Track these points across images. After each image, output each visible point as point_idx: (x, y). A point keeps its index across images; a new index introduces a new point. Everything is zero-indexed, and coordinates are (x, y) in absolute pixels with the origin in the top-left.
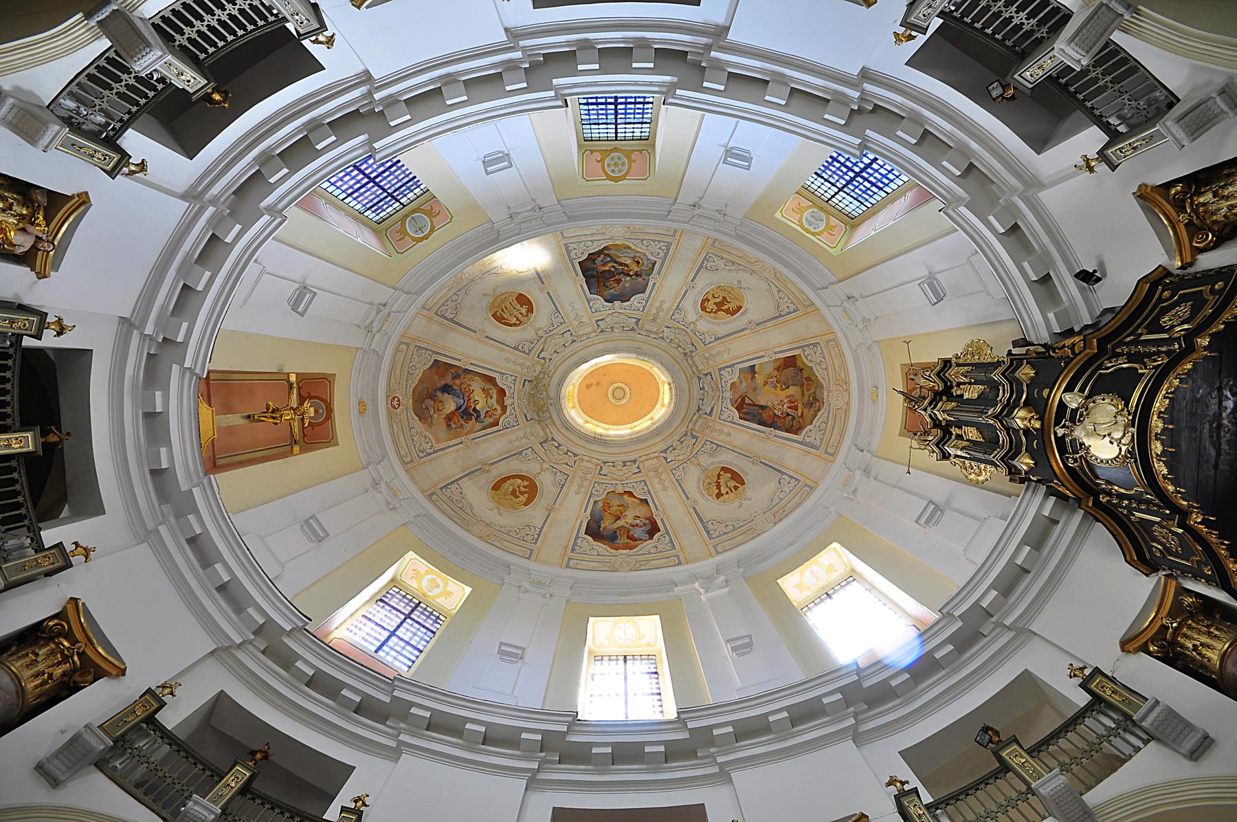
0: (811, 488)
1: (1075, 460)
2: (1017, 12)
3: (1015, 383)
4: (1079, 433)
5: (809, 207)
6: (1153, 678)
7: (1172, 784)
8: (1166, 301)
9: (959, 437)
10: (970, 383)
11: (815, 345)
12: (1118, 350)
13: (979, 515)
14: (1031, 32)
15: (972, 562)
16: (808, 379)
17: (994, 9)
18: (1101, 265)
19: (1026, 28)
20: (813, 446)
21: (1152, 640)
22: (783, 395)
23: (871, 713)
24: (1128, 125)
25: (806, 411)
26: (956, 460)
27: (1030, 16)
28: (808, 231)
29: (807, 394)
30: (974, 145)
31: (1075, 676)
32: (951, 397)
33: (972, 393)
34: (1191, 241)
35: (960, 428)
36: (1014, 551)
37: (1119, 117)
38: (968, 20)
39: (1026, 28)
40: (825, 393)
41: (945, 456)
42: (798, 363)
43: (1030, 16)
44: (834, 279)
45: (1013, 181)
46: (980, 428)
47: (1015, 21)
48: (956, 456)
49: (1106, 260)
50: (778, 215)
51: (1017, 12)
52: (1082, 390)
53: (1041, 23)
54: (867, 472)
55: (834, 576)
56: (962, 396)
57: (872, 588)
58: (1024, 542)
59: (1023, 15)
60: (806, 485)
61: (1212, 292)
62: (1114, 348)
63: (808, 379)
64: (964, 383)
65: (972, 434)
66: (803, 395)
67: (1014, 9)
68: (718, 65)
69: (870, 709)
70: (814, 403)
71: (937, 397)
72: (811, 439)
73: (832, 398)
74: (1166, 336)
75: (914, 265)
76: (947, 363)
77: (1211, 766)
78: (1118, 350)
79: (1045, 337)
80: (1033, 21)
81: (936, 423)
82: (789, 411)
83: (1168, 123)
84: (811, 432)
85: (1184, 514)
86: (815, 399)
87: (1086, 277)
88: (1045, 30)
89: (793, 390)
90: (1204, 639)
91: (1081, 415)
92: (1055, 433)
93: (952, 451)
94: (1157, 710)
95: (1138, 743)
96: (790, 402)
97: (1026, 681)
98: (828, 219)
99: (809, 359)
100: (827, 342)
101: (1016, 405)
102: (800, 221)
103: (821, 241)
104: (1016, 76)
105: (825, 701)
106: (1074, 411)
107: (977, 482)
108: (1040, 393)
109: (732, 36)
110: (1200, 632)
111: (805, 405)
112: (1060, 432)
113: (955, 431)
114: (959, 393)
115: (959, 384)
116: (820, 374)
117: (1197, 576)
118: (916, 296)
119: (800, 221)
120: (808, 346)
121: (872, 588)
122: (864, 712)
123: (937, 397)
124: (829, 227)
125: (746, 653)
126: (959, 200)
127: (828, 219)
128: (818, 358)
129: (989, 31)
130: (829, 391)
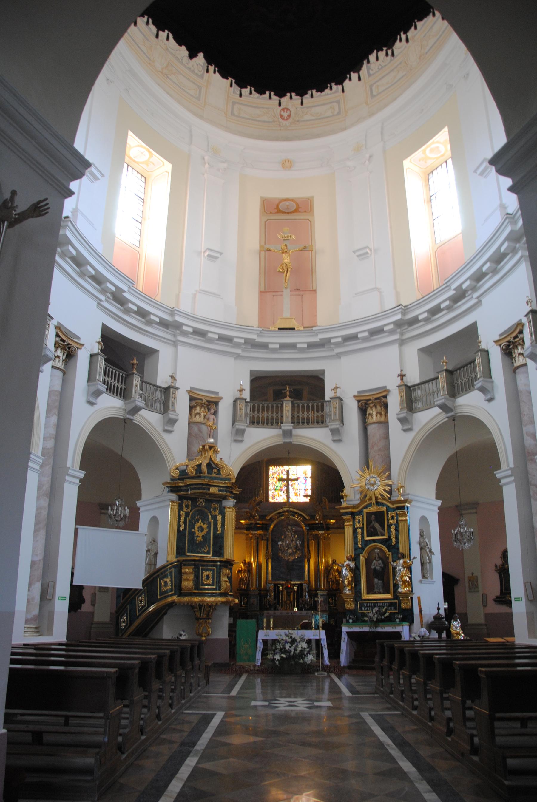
6: (181, 404)
39: (459, 380)
122: (110, 299)
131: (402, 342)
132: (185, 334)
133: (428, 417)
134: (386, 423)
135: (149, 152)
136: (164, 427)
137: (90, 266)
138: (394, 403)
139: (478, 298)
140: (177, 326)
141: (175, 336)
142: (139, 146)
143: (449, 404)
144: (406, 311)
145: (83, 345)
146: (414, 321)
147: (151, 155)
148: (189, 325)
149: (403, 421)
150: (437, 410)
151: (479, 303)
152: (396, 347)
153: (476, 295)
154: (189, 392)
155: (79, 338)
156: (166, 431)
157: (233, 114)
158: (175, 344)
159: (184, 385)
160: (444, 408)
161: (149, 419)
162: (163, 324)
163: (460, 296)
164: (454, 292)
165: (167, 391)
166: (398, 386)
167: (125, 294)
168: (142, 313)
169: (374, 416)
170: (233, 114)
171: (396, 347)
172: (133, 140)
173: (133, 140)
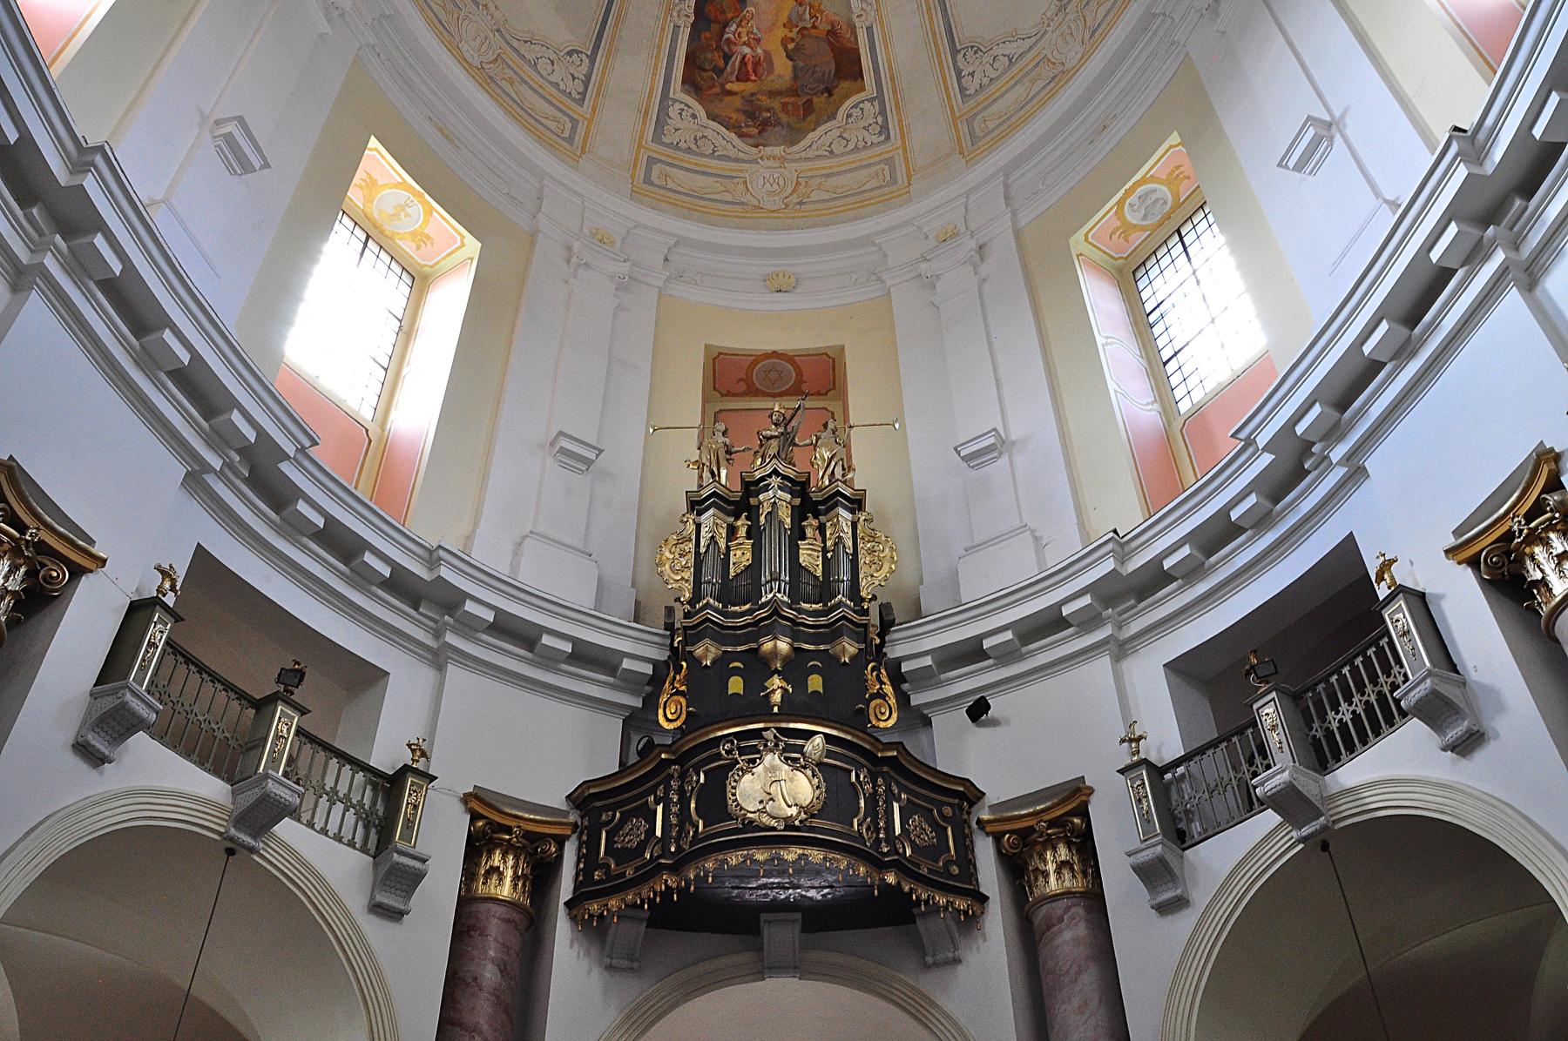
0: (570, 140)
1: (728, 752)
2: (1354, 712)
3: (833, 633)
4: (771, 759)
5: (1176, 195)
6: (440, 835)
7: (334, 895)
8: (940, 813)
9: (732, 532)
10: (825, 550)
11: (885, 128)
12: (880, 781)
13: (584, 523)
14: (1323, 716)
15: (517, 553)
16: (808, 108)
17: (1369, 688)
18: (994, 723)
19: (1331, 714)
20: (660, 124)
21: (490, 823)
22: (773, 44)
23: (238, 482)
24: (1170, 783)
25: (737, 102)
26: (691, 527)
27: (1343, 726)
28: (1128, 193)
29: (776, 104)
30: (1202, 588)
31: (413, 751)
32: (799, 514)
33: (809, 557)
34: (1012, 832)
35: (749, 537)
36: (559, 632)
37: (1183, 775)
38: (1370, 652)
39: (1331, 714)
40: (778, 151)
41: (696, 505)
42: (845, 85)
43: (1343, 726)
44: (1023, 222)
45: (1136, 626)
46: (754, 568)
47: (1344, 706)
48: (698, 526)
49: (998, 729)
50: (1175, 138)
51: (1354, 712)
52: (829, 754)
53: (1329, 734)
54: (624, 285)
55: (407, 246)
56: (803, 537)
57: (407, 331)
58: (575, 641)
59: (1348, 717)
60: (575, 123)
61: (948, 863)
62: (883, 775)
63: (808, 108)
64: (824, 541)
65: (741, 557)
66: (773, 94)
67: (1360, 710)
68: (1475, 255)
69: (246, 481)
70: (755, 123)
71: (799, 487)
72: (674, 120)
73: (768, 170)
74: (898, 831)
75: (1030, 418)
76: (856, 504)
77: (375, 930)
78: (880, 781)
79: (894, 651)
80: (1335, 726)
81: (752, 487)
82: (736, 61)
83: (1159, 848)
84: (689, 117)
85: (674, 869)
86: (764, 125)
87: (978, 710)
88: (1319, 734)
89: (783, 68)
90: (509, 873)
91: (795, 760)
92: (766, 729)
93: (708, 518)
94: (417, 864)
95: (358, 839)
96: (757, 64)
97: (368, 677)
98: (1143, 229)
99: (855, 111)
100: (889, 162)
101: (795, 636)
102: (1153, 179)
103: (1104, 216)
104: (1274, 694)
105: (236, 416)
106: (800, 749)
107: (661, 564)
108: (815, 670)
109: (1513, 298)
110: (515, 867)
111: (750, 99)
112: (769, 735)
113: (742, 524)
114: (809, 532)
115: (821, 529)
116: (821, 136)
117: (588, 859)
118: (976, 423)
119: (1153, 179)
120: (883, 112)
121: (407, 331)
122: (237, 474)
123: (799, 487)
124: (1128, 228)
125: (229, 167)
126: (1122, 559)
127: (1143, 229)
128: (856, 135)
129: (1346, 670)
130: (782, 160)
131: (1121, 649)
132: (470, 627)
133: (1240, 852)
134: (1094, 899)
135: (424, 202)
136: (372, 897)
137: (105, 236)
138: (1118, 830)
139: (1348, 458)
140: (449, 602)
141: (438, 635)
142: (397, 185)
143: (1308, 784)
144: (1127, 549)
145: (104, 561)
146: (1155, 579)
147: (429, 211)
148: (483, 603)
149: (1153, 873)
150: (1269, 819)
151: (1356, 473)
152: (1104, 662)
153: (1338, 452)
154: (466, 799)
155: (92, 542)
156: (377, 909)
157: (647, 180)
158: (438, 658)
159: (455, 773)
160: (1291, 804)
161: (319, 853)
162: (401, 586)
163: (1294, 464)
164: (1267, 458)
165: (390, 785)
166: (1121, 772)
167: (285, 467)
168: (341, 544)
169: (1052, 878)
170: (647, 180)
171: (1104, 662)
172: (378, 160)
173: (378, 160)
